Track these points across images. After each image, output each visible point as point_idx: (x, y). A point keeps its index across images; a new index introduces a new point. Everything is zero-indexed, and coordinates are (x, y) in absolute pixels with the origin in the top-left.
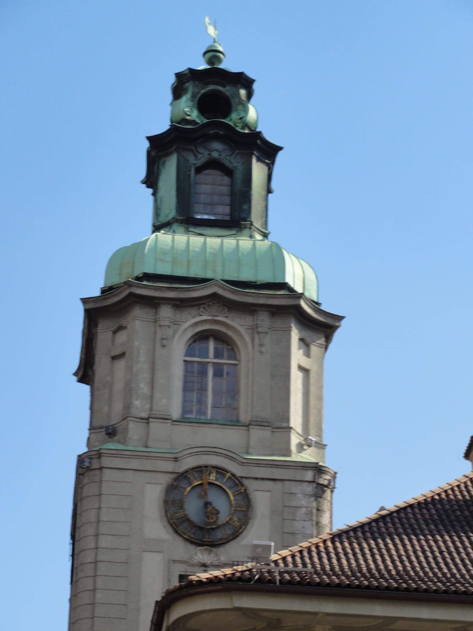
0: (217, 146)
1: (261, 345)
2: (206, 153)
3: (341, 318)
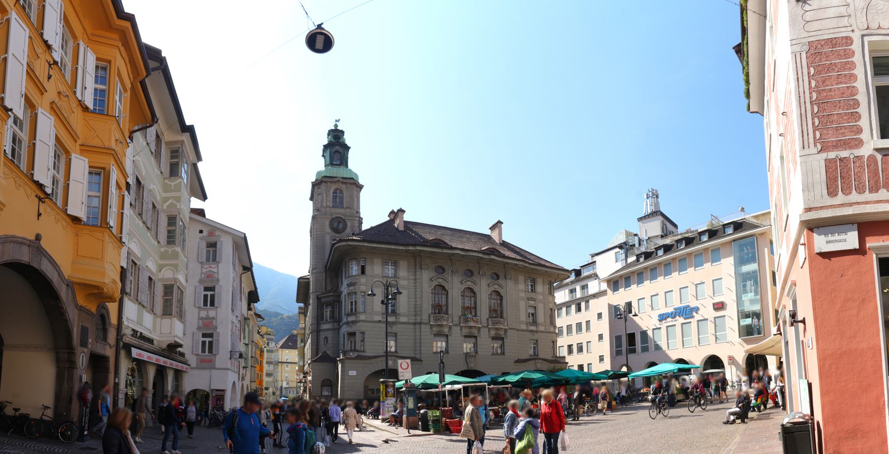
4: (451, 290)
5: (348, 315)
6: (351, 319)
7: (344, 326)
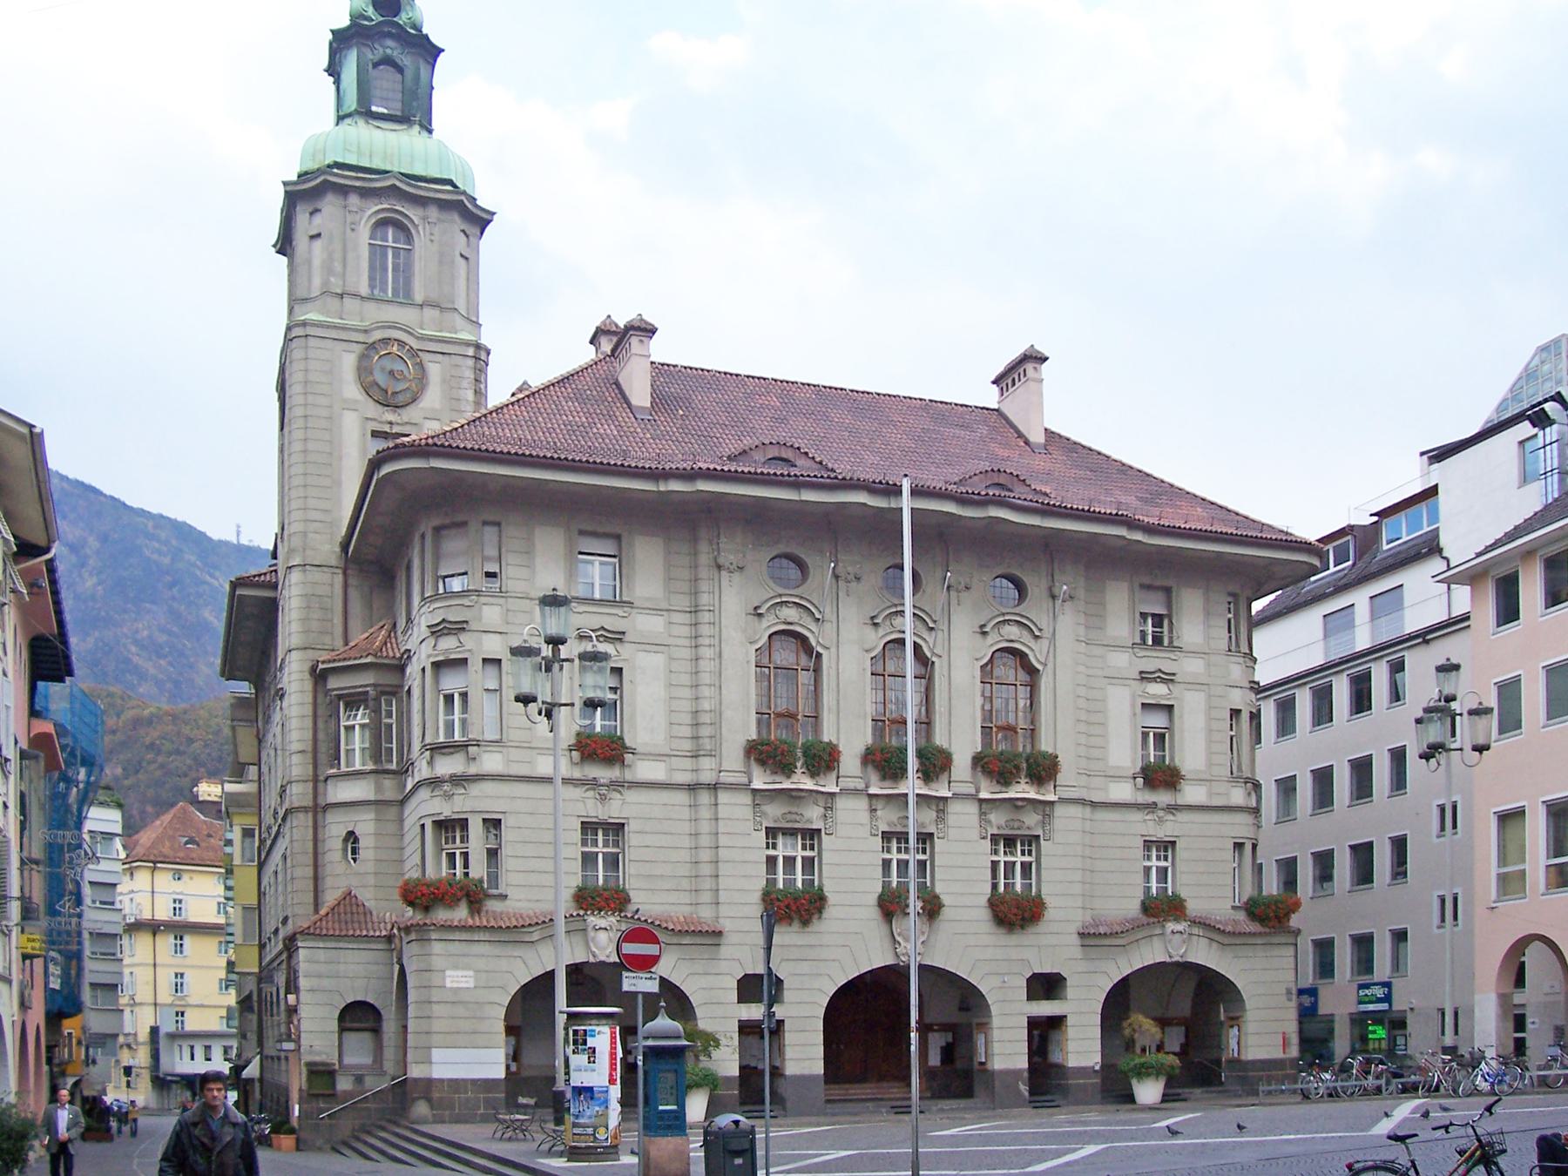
0: (389, 43)
1: (432, 234)
2: (381, 50)
3: (494, 213)
4: (833, 650)
5: (437, 749)
6: (447, 766)
7: (424, 793)
